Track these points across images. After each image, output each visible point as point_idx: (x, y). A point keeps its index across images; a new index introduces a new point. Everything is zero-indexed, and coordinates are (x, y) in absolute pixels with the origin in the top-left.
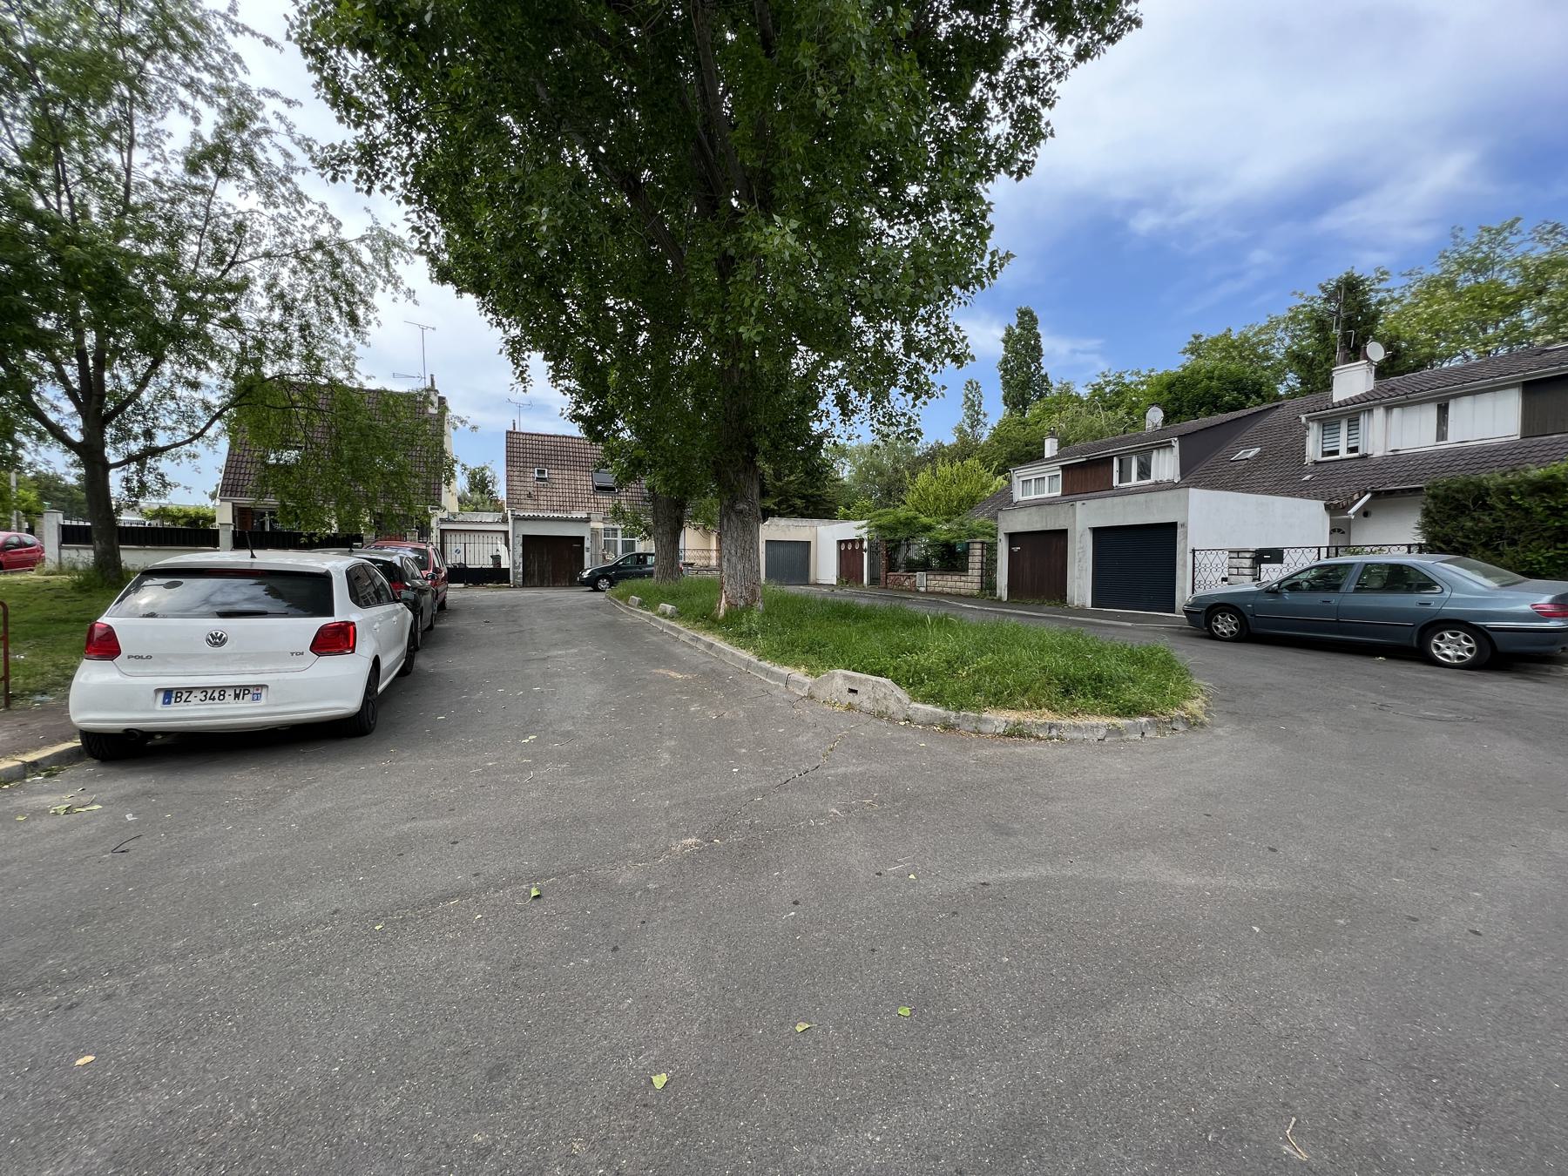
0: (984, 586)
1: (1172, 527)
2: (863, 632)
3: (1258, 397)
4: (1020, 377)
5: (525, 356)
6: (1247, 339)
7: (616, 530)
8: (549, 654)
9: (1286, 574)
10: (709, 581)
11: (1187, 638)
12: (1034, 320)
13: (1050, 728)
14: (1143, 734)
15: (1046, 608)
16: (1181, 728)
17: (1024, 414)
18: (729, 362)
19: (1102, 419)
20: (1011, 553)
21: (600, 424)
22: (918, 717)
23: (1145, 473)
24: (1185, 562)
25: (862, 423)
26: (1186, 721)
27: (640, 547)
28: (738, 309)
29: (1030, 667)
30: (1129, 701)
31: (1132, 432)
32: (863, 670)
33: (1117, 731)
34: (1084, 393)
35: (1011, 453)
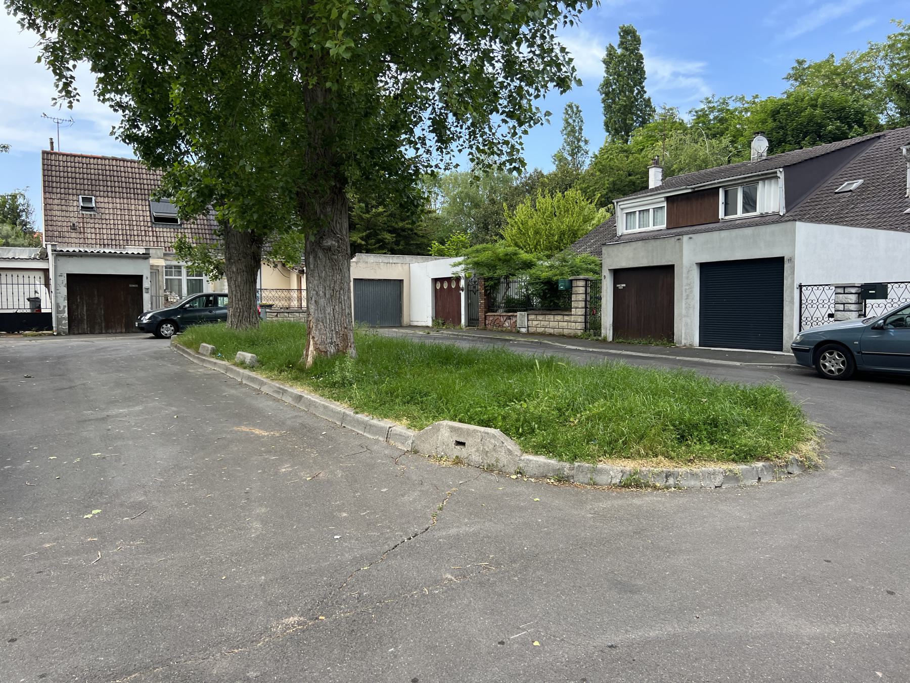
0: (588, 325)
1: (780, 261)
2: (466, 379)
3: (859, 127)
4: (622, 101)
5: (70, 65)
6: (849, 66)
7: (179, 267)
8: (109, 413)
9: (890, 310)
10: (292, 326)
11: (805, 378)
12: (637, 40)
13: (667, 477)
14: (759, 479)
15: (653, 347)
16: (796, 471)
17: (627, 141)
18: (313, 81)
19: (706, 148)
20: (616, 291)
21: (159, 146)
22: (531, 470)
23: (749, 205)
24: (793, 298)
25: (460, 151)
26: (801, 464)
27: (209, 287)
28: (324, 21)
29: (645, 412)
30: (745, 445)
31: (736, 162)
32: (470, 421)
33: (732, 477)
34: (688, 119)
35: (614, 183)
